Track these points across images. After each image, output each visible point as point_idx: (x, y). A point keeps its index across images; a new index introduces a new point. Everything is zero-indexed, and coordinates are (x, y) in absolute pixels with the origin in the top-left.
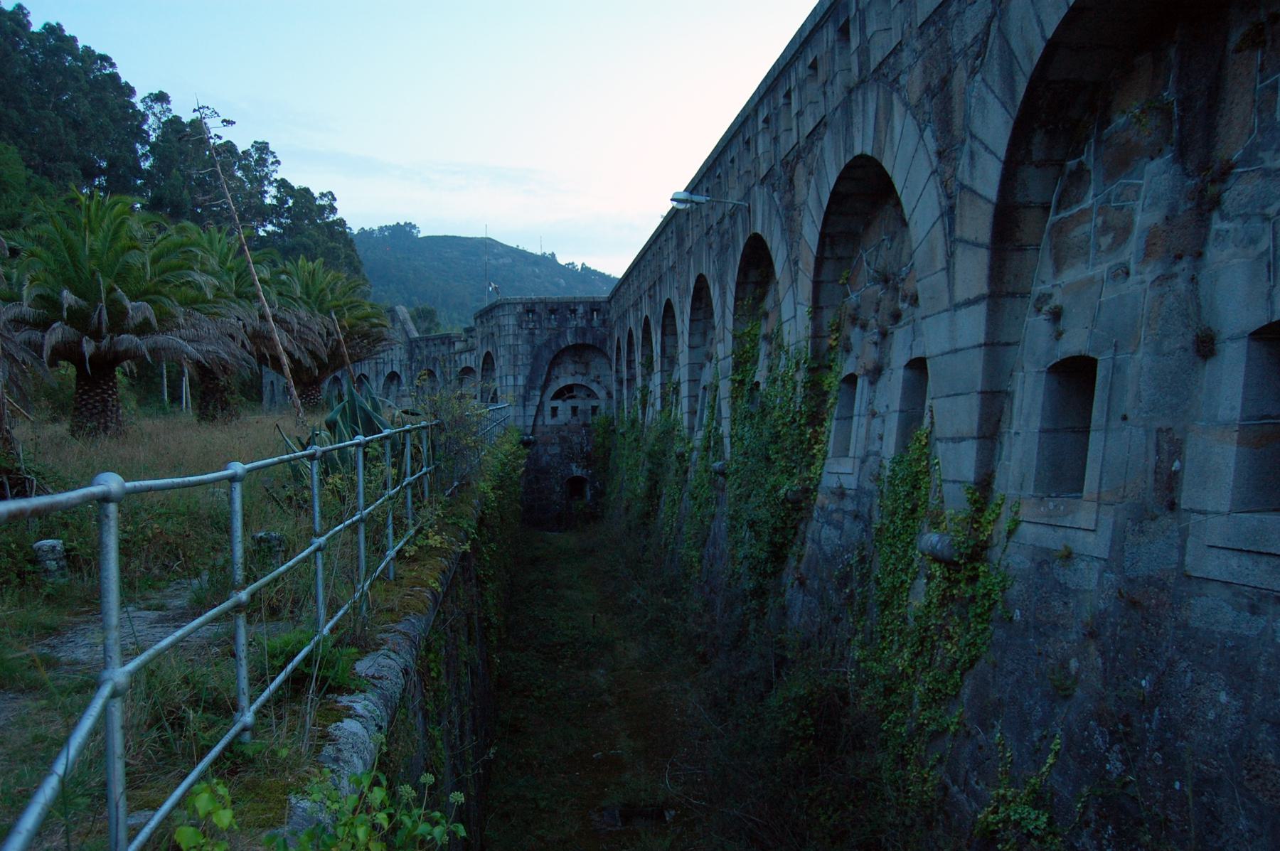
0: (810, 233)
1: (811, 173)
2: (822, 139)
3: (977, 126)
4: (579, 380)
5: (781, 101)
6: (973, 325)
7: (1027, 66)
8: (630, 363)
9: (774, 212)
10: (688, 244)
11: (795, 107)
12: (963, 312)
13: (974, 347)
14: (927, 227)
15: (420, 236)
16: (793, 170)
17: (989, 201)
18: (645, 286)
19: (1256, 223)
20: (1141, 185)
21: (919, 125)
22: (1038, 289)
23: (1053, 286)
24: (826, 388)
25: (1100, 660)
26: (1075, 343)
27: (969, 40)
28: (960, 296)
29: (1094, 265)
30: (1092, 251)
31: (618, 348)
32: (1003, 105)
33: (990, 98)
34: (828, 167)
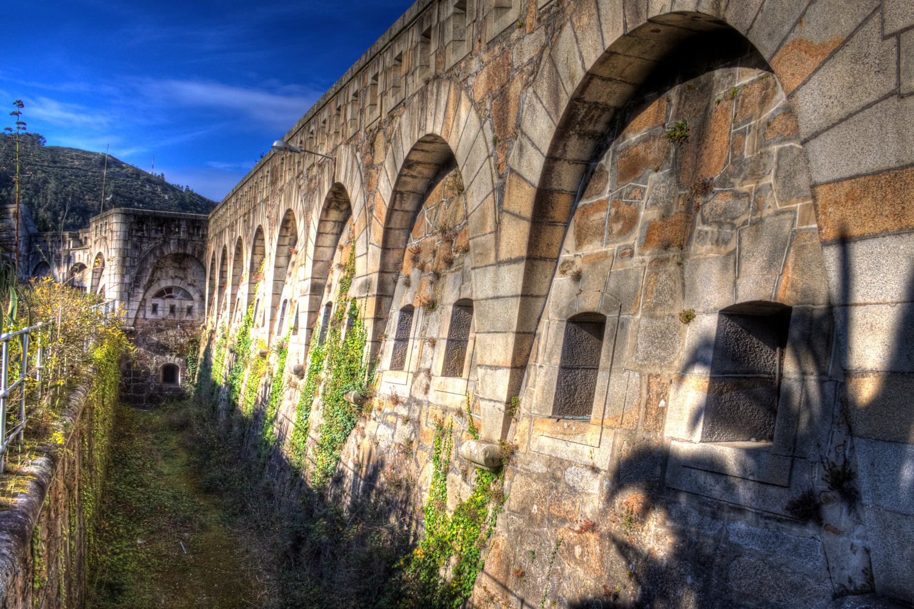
0: (385, 187)
1: (389, 141)
2: (401, 116)
3: (527, 125)
4: (178, 283)
5: (369, 81)
6: (511, 280)
7: (569, 90)
8: (223, 273)
9: (356, 169)
10: (280, 184)
11: (380, 89)
12: (504, 269)
13: (513, 296)
14: (481, 198)
15: (46, 145)
16: (374, 137)
17: (533, 185)
18: (241, 212)
19: (727, 230)
20: (645, 189)
21: (480, 119)
22: (564, 256)
23: (575, 256)
25: (598, 547)
26: (591, 302)
27: (525, 61)
28: (503, 256)
29: (607, 244)
30: (606, 233)
31: (213, 259)
32: (549, 113)
33: (539, 107)
34: (404, 139)
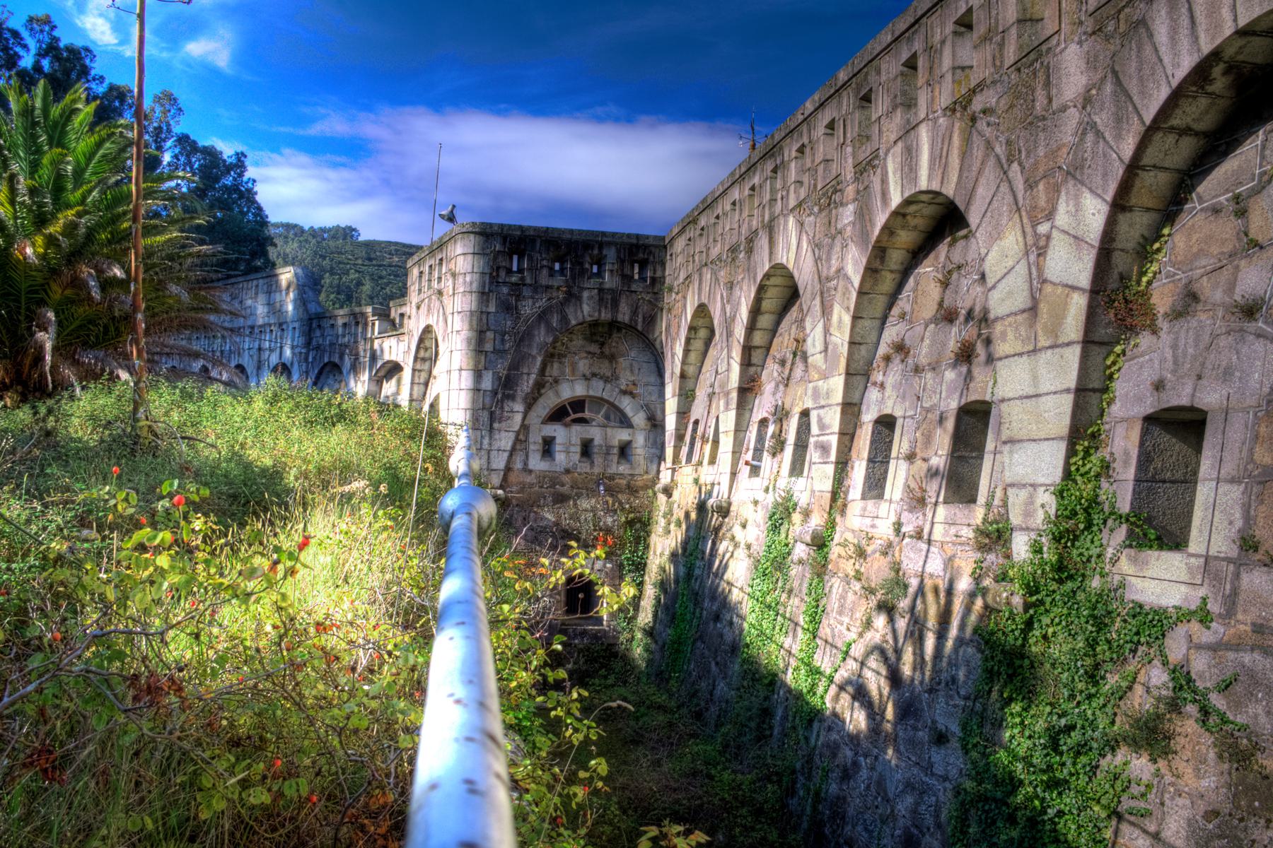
6: (1061, 370)
15: (360, 239)
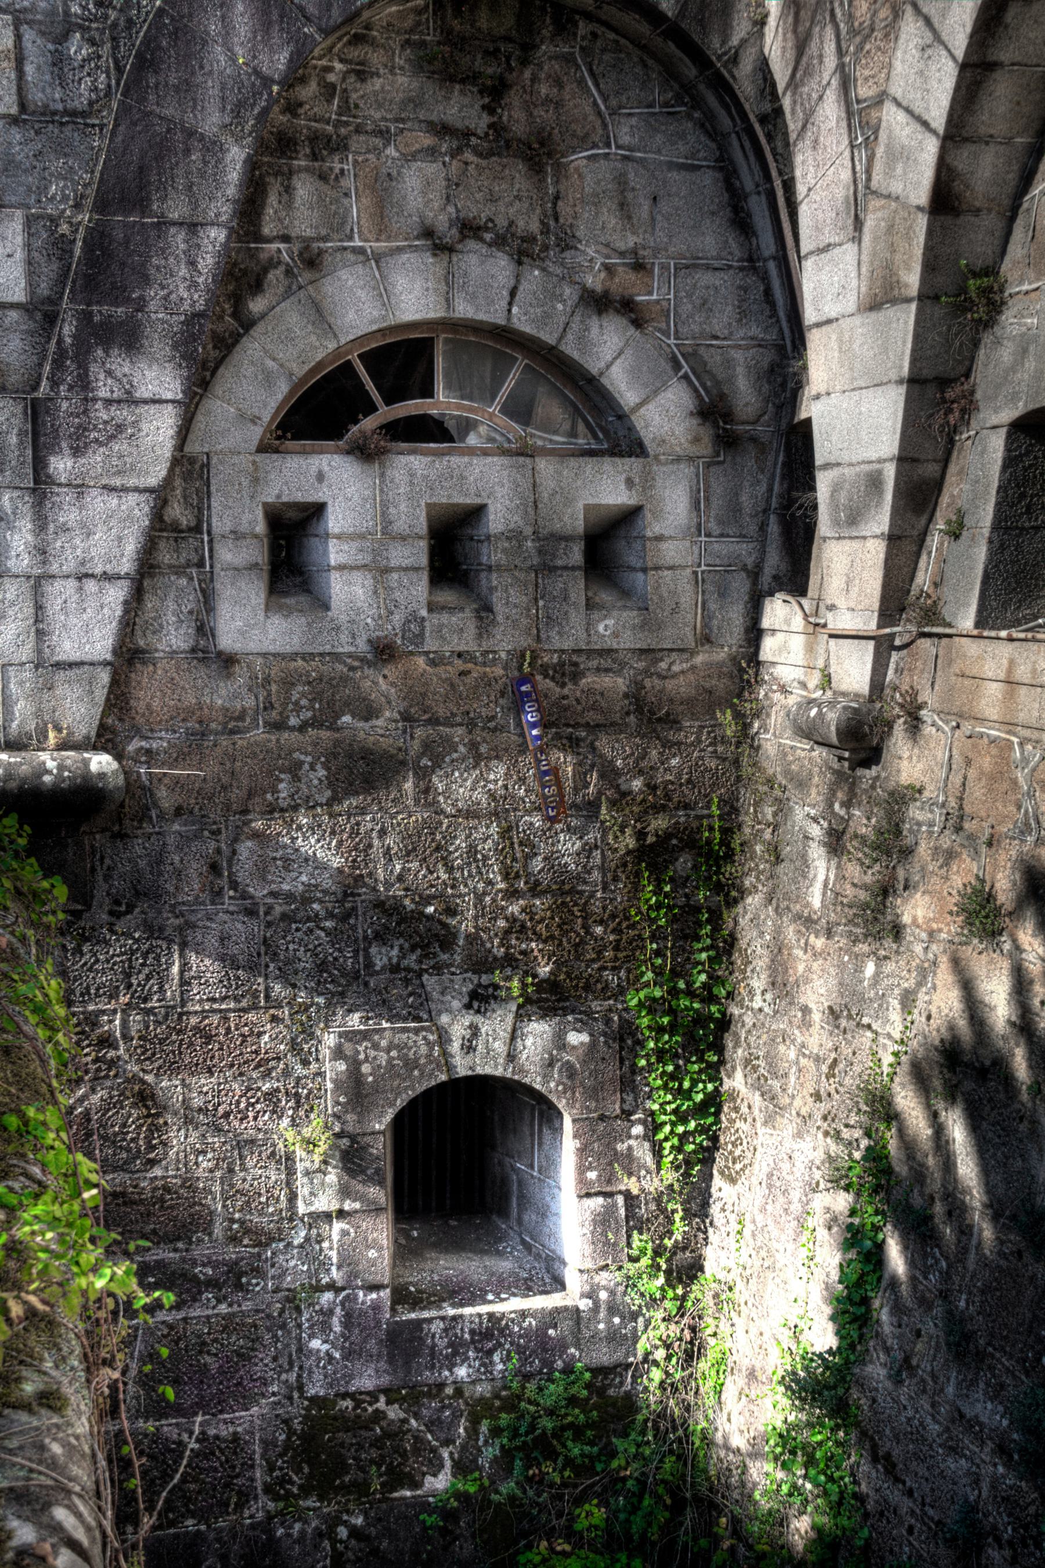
4: (487, 288)
24: (909, 841)
